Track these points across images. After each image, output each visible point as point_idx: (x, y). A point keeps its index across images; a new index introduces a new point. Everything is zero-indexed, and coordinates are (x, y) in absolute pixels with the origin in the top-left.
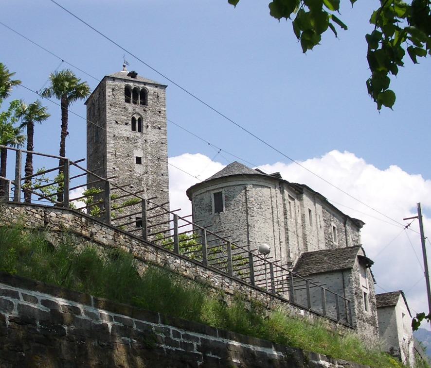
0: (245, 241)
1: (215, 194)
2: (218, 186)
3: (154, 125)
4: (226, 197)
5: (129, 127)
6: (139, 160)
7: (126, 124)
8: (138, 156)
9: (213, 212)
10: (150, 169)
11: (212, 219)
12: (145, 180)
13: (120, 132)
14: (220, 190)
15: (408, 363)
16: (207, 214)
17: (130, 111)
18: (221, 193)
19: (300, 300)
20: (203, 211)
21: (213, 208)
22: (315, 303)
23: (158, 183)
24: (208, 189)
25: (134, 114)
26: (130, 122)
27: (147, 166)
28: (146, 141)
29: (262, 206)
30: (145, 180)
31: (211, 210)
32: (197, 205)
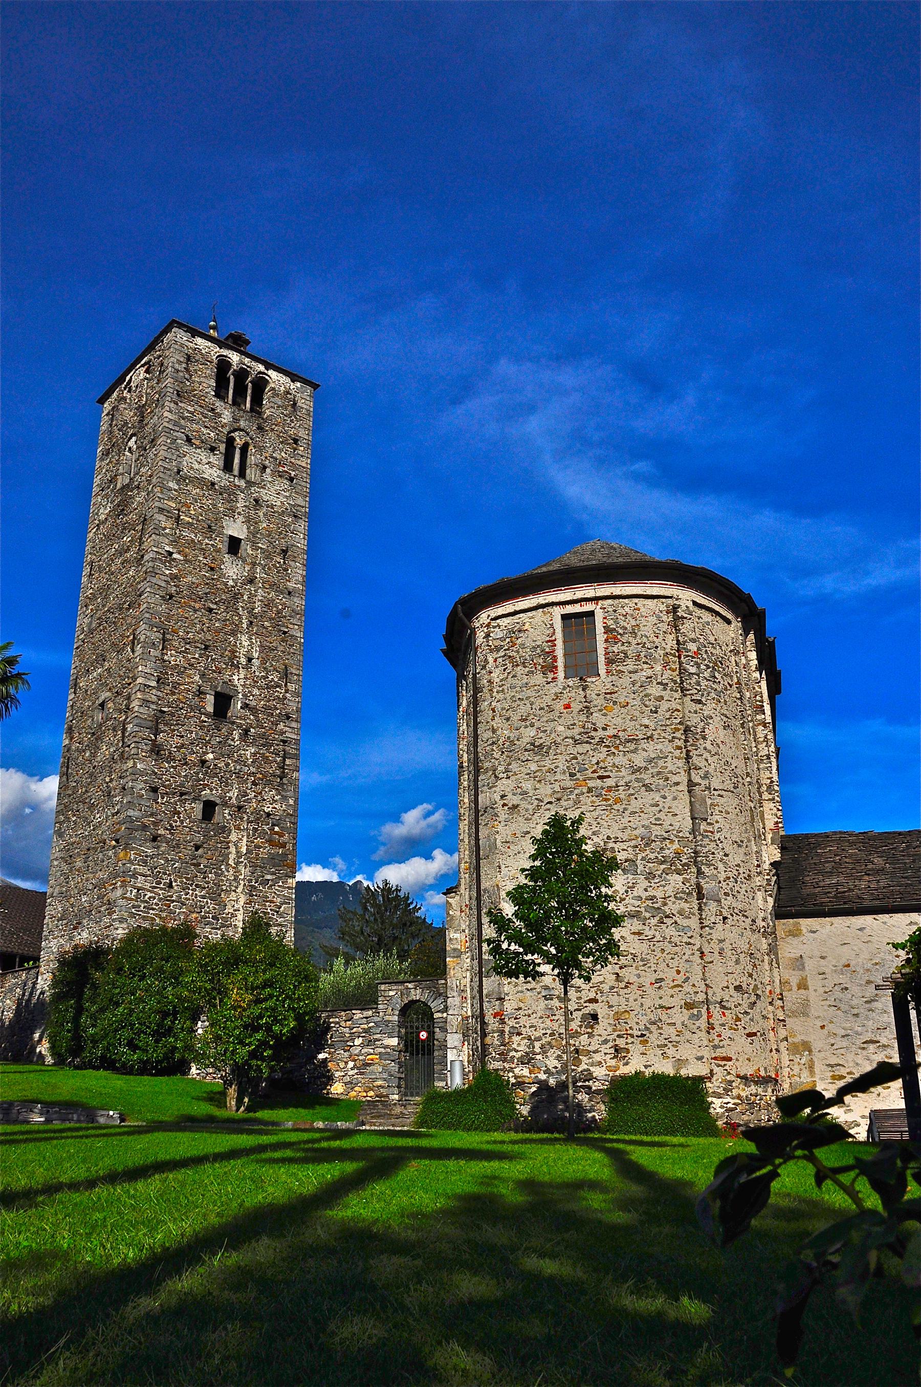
0: (675, 779)
1: (564, 617)
2: (579, 594)
3: (281, 469)
4: (607, 630)
5: (217, 460)
6: (234, 545)
7: (213, 449)
8: (236, 535)
9: (561, 674)
10: (259, 573)
11: (557, 696)
12: (245, 597)
13: (196, 466)
14: (588, 607)
15: (917, 1168)
16: (538, 679)
17: (225, 421)
18: (591, 614)
19: (822, 990)
20: (520, 670)
21: (560, 663)
22: (875, 1004)
23: (279, 612)
24: (542, 599)
25: (235, 430)
26: (222, 447)
27: (254, 564)
28: (256, 501)
29: (717, 674)
30: (245, 597)
31: (553, 668)
32: (498, 649)
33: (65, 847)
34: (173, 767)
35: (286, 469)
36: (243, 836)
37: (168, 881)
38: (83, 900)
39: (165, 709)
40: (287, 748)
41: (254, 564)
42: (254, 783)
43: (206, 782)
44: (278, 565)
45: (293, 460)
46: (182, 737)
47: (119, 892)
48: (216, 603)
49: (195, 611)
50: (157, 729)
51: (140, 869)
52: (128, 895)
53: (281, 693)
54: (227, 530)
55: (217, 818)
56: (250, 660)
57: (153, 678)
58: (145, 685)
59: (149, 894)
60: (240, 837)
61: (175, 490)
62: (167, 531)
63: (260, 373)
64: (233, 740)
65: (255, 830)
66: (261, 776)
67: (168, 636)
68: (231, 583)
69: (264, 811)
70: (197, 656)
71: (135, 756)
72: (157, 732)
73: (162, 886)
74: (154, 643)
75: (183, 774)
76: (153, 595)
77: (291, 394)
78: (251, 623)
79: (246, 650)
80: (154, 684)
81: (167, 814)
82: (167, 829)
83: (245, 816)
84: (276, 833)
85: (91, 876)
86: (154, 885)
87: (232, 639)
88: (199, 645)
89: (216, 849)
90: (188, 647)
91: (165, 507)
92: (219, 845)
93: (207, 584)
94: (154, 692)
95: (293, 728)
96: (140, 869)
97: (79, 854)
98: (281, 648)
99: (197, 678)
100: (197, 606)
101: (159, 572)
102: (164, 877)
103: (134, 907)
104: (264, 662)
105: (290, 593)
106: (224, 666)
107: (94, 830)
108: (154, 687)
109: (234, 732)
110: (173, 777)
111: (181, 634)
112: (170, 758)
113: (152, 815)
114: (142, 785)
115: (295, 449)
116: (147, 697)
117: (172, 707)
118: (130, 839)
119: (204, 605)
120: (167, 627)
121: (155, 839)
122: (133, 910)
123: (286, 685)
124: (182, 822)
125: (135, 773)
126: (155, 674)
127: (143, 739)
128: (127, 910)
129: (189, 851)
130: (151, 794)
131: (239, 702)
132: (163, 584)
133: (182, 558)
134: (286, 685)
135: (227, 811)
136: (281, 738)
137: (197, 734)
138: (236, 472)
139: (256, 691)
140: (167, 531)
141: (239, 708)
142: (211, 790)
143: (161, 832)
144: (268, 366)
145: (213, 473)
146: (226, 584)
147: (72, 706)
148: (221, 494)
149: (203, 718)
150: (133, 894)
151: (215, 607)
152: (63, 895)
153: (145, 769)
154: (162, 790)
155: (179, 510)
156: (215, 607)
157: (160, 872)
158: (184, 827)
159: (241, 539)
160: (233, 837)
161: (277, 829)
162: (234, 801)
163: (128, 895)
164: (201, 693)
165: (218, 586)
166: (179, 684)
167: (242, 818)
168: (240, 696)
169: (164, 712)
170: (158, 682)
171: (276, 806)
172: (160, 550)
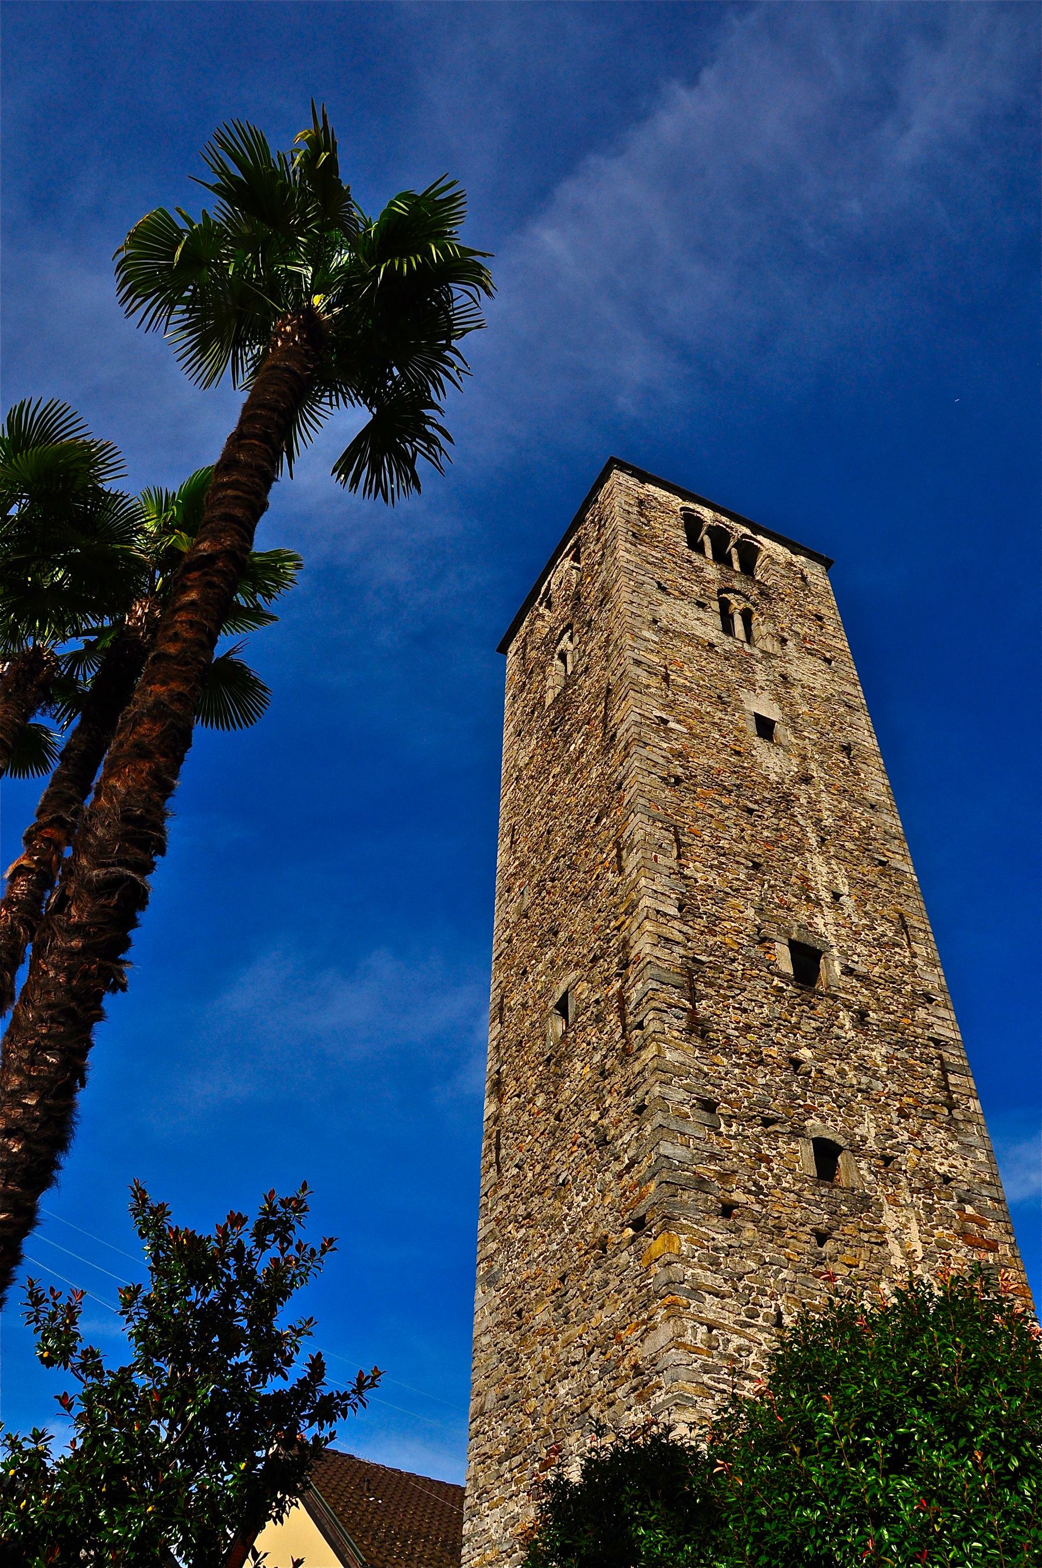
12: (803, 801)
13: (681, 620)
30: (803, 801)
33: (503, 1300)
34: (737, 1065)
35: (815, 647)
36: (908, 1220)
37: (772, 1311)
38: (562, 1392)
39: (703, 958)
40: (945, 1054)
41: (804, 758)
42: (903, 1114)
43: (809, 1102)
44: (842, 765)
45: (822, 638)
46: (745, 1011)
47: (664, 1333)
48: (756, 802)
49: (725, 808)
50: (693, 989)
51: (709, 1279)
52: (688, 1338)
53: (905, 957)
54: (750, 705)
55: (843, 1177)
56: (836, 896)
57: (669, 901)
58: (658, 912)
59: (737, 1341)
60: (903, 1220)
61: (655, 643)
62: (653, 690)
63: (745, 536)
64: (841, 1027)
65: (930, 1209)
66: (910, 1100)
67: (684, 839)
68: (773, 777)
69: (936, 1172)
70: (742, 877)
71: (658, 1036)
72: (694, 997)
73: (760, 1321)
74: (660, 846)
75: (762, 1081)
76: (645, 773)
77: (795, 567)
78: (823, 840)
79: (825, 879)
80: (673, 911)
81: (742, 1160)
82: (750, 1192)
83: (902, 1177)
84: (971, 1219)
85: (578, 1330)
86: (743, 1317)
87: (796, 859)
88: (743, 861)
89: (860, 1244)
90: (723, 859)
91: (643, 660)
92: (865, 1237)
93: (735, 772)
94: (676, 924)
95: (943, 1019)
96: (709, 1279)
97: (539, 1299)
98: (884, 886)
99: (750, 913)
100: (725, 801)
101: (649, 742)
102: (763, 1300)
103: (706, 1369)
104: (861, 902)
105: (872, 807)
106: (795, 900)
107: (572, 1231)
108: (675, 918)
109: (841, 1013)
110: (742, 1086)
111: (707, 838)
112: (729, 1048)
113: (713, 1157)
114: (682, 1095)
115: (822, 628)
116: (665, 931)
117: (715, 956)
118: (674, 1206)
119: (737, 801)
120: (682, 825)
121: (727, 1210)
122: (705, 1378)
123: (909, 945)
124: (778, 1179)
125: (665, 1072)
126: (673, 896)
127: (670, 1006)
128: (691, 1375)
129: (805, 1242)
130: (705, 1115)
131: (836, 963)
132: (661, 761)
133: (685, 730)
134: (909, 945)
135: (862, 1165)
136: (927, 1033)
137: (772, 1010)
138: (743, 637)
139: (860, 948)
140: (653, 690)
141: (839, 973)
142: (823, 1119)
143: (738, 1196)
144: (756, 529)
145: (709, 628)
146: (766, 778)
147: (497, 1047)
148: (727, 659)
149: (776, 981)
150: (699, 1336)
151: (756, 807)
152: (510, 1400)
153: (682, 1064)
154: (724, 1109)
155: (665, 667)
156: (756, 807)
157: (751, 1289)
158: (784, 1189)
159: (775, 722)
160: (890, 1219)
161: (969, 1209)
162: (871, 1144)
163: (688, 1338)
164: (764, 940)
165: (755, 778)
166: (718, 918)
167: (895, 1182)
168: (835, 952)
169: (702, 963)
170: (680, 909)
171: (955, 1163)
172: (646, 714)
